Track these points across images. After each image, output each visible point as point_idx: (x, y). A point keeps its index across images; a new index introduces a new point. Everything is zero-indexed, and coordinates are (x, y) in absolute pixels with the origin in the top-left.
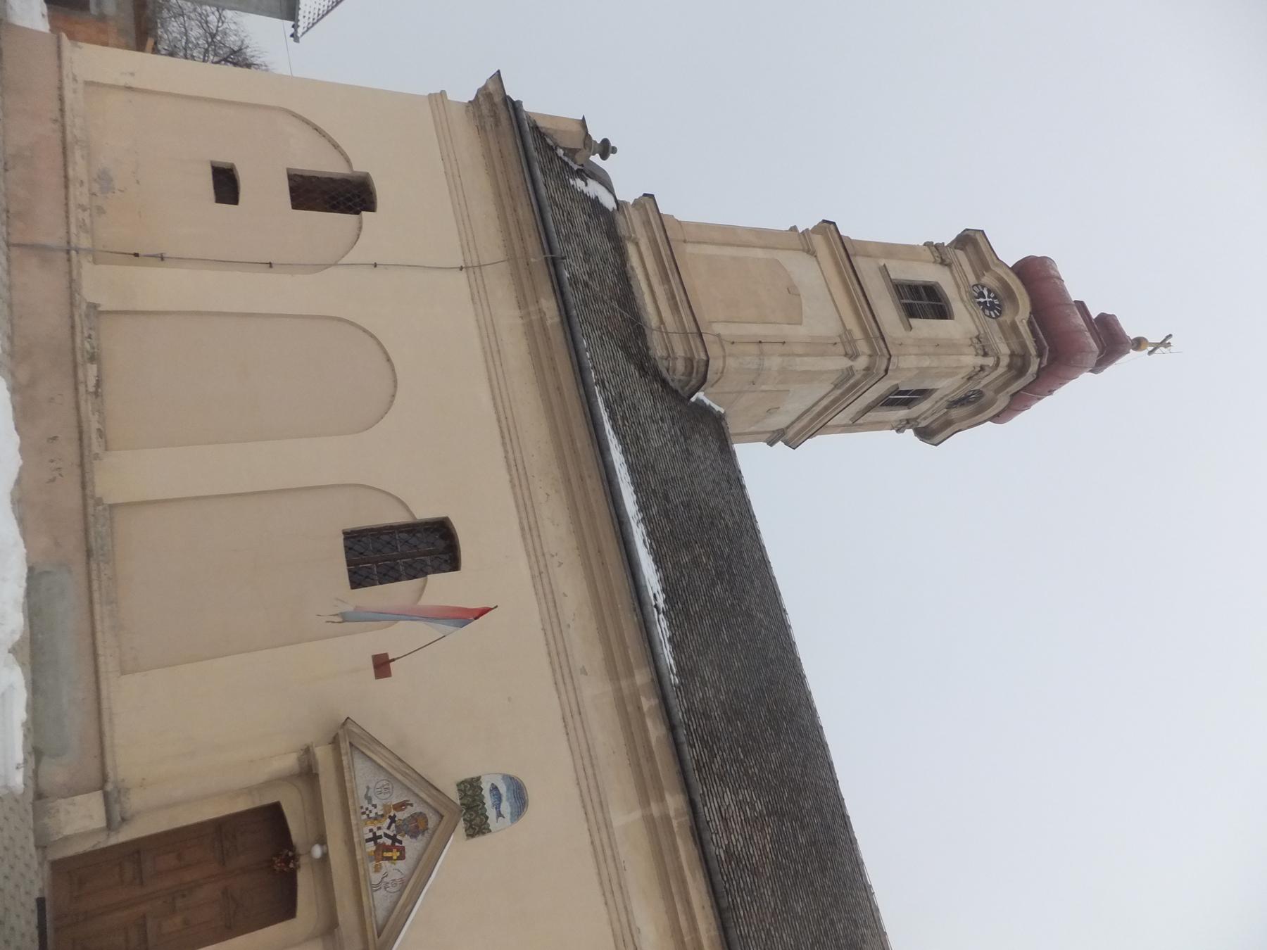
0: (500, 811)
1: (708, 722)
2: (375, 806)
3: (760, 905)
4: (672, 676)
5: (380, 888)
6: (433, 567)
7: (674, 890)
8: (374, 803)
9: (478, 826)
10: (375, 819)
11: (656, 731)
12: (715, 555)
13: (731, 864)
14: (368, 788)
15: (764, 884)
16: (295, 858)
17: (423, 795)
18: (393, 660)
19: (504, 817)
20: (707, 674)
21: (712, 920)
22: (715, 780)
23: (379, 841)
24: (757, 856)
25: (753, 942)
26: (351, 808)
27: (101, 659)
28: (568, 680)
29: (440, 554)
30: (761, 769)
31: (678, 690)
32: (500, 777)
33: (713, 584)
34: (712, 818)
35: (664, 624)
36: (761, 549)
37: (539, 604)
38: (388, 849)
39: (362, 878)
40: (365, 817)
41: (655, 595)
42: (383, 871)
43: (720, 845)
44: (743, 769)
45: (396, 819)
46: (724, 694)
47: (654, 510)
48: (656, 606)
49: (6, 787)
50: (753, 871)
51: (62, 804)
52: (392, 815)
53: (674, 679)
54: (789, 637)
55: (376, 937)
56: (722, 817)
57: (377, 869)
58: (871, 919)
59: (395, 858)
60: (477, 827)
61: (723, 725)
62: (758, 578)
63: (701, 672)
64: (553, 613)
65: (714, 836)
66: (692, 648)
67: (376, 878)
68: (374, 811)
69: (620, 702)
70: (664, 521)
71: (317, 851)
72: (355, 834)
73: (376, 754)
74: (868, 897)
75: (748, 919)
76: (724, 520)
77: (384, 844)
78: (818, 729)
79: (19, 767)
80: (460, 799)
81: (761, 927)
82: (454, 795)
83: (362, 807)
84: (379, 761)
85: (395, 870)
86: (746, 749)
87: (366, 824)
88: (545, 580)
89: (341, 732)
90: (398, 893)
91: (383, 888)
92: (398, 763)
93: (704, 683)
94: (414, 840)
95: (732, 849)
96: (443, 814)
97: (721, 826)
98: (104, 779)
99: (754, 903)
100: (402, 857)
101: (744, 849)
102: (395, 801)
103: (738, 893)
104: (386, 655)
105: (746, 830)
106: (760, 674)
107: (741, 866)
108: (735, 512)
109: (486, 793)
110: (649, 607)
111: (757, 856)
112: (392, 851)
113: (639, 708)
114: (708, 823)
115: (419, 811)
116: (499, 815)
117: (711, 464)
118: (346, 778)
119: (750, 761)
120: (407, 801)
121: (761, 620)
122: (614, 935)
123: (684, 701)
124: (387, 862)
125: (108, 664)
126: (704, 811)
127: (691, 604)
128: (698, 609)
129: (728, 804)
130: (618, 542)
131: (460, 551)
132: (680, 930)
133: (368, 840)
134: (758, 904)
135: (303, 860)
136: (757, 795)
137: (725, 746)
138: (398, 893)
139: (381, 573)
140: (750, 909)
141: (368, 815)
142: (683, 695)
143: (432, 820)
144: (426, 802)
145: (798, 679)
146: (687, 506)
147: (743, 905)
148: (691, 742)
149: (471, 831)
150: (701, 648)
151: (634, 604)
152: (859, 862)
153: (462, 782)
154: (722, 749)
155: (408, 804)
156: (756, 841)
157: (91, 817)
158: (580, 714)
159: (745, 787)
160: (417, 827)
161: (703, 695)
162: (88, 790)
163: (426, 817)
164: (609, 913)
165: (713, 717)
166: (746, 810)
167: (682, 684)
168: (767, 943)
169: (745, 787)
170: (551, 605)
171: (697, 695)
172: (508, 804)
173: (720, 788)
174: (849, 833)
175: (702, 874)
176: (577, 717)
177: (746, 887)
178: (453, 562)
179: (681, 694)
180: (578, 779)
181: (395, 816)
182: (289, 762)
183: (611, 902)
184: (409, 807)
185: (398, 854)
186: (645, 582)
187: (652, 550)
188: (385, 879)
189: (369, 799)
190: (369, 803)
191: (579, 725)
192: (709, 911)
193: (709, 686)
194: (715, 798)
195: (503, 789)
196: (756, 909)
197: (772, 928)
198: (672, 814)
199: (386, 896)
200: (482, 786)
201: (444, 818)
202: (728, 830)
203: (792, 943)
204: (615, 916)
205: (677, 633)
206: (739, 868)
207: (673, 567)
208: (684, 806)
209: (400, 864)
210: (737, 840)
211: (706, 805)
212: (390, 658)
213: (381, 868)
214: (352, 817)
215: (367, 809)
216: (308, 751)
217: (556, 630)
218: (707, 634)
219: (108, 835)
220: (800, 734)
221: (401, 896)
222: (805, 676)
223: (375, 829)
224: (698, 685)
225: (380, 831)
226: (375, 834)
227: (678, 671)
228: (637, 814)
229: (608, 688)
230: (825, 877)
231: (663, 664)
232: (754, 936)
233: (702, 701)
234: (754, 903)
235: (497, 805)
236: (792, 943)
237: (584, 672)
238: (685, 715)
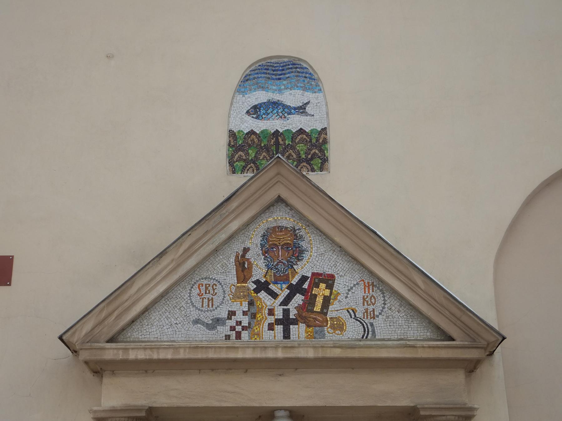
0: (295, 109)
2: (232, 314)
5: (372, 325)
8: (225, 315)
9: (310, 150)
14: (197, 322)
17: (234, 226)
19: (308, 103)
23: (292, 316)
26: (223, 355)
32: (239, 97)
40: (245, 335)
42: (344, 315)
45: (263, 280)
57: (339, 326)
59: (327, 292)
68: (239, 316)
72: (270, 354)
77: (298, 308)
82: (240, 179)
83: (228, 337)
87: (258, 334)
89: (84, 355)
90: (387, 295)
91: (372, 321)
92: (166, 260)
94: (306, 256)
100: (329, 280)
102: (232, 278)
109: (259, 126)
112: (315, 296)
116: (302, 110)
118: (169, 356)
120: (237, 257)
133: (287, 335)
141: (244, 328)
153: (231, 163)
155: (243, 256)
160: (286, 246)
163: (274, 228)
172: (287, 92)
181: (257, 282)
185: (323, 286)
188: (359, 315)
189: (218, 321)
190: (224, 324)
199: (388, 317)
209: (340, 285)
213: (338, 319)
214: (240, 355)
221: (394, 292)
223: (271, 319)
226: (278, 322)
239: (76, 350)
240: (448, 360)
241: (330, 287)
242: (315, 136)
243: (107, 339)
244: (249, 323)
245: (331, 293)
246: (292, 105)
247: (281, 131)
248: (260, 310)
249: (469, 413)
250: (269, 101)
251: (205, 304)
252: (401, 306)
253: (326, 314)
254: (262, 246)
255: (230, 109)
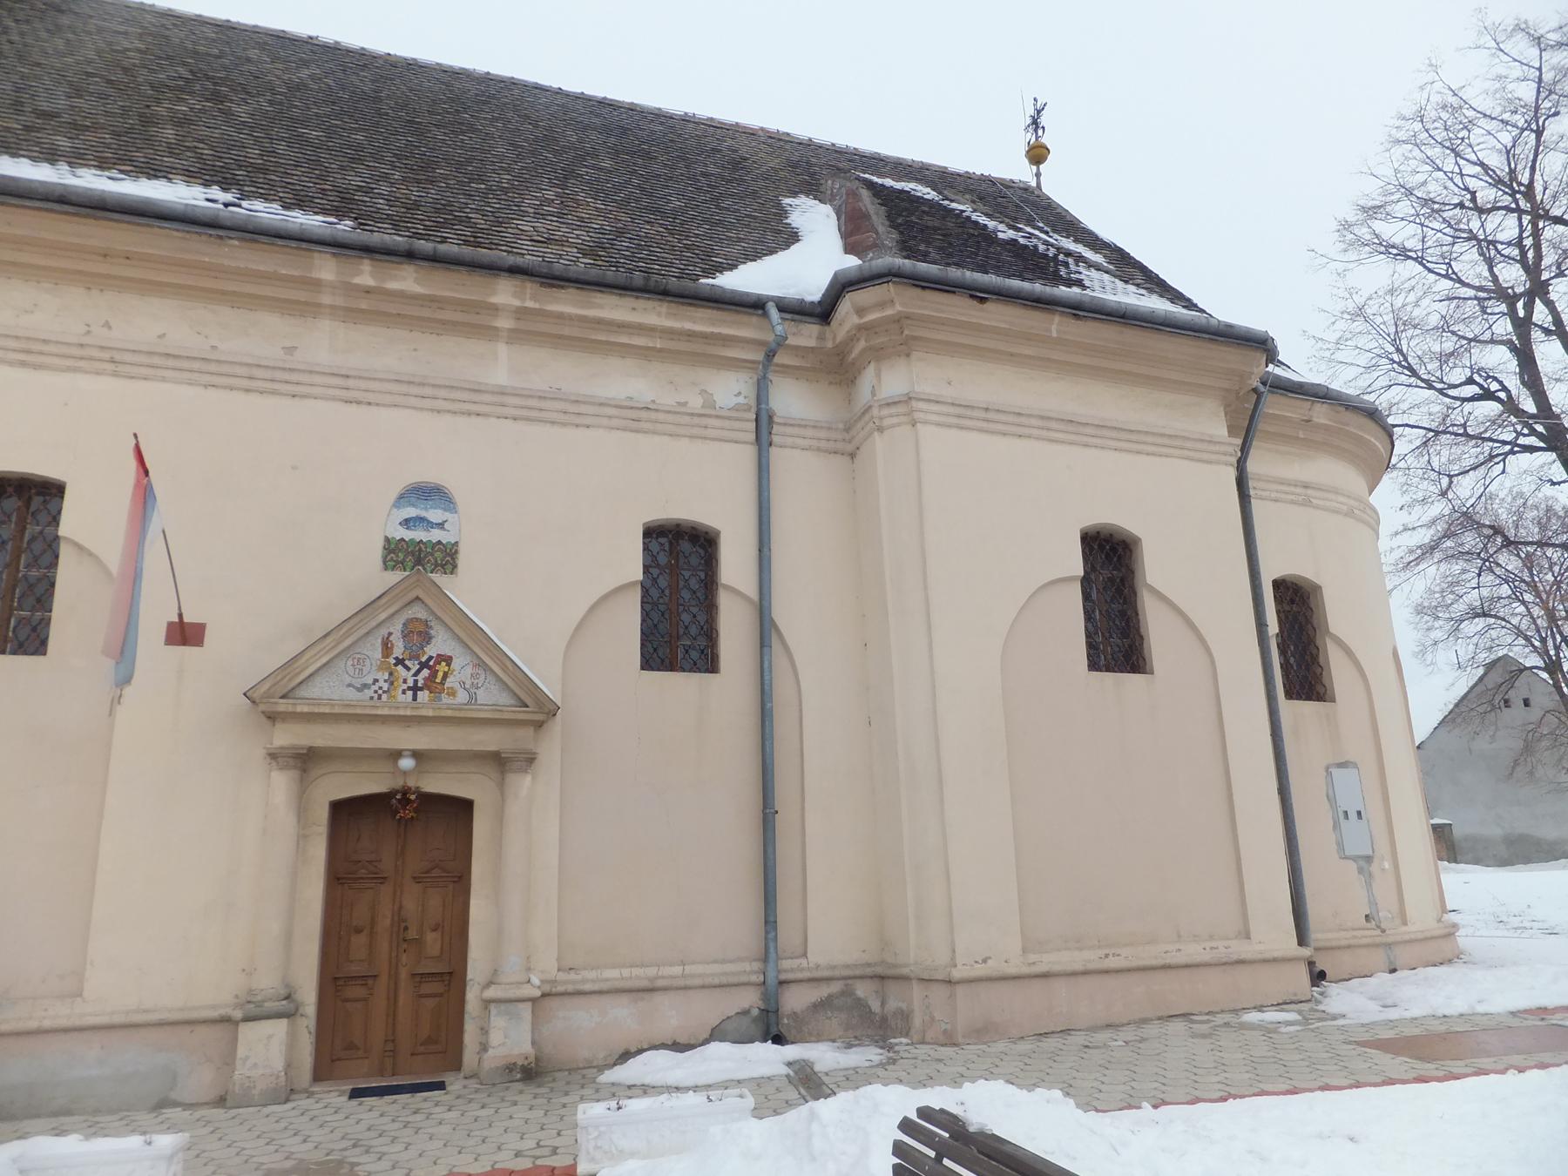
0: (436, 524)
1: (421, 208)
2: (376, 681)
3: (657, 243)
4: (338, 226)
5: (475, 693)
6: (49, 524)
7: (604, 338)
8: (371, 682)
10: (392, 683)
11: (407, 280)
12: (182, 90)
13: (600, 256)
14: (349, 685)
15: (638, 229)
16: (405, 792)
17: (383, 616)
18: (180, 616)
19: (446, 521)
20: (357, 181)
21: (650, 304)
22: (497, 231)
23: (419, 685)
24: (604, 223)
25: (691, 268)
26: (367, 711)
27: (47, 1024)
28: (294, 377)
29: (28, 508)
30: (508, 171)
31: (362, 227)
33: (228, 114)
34: (541, 254)
35: (258, 205)
36: (200, 21)
37: (164, 379)
38: (433, 674)
39: (457, 714)
40: (384, 697)
41: (208, 200)
42: (457, 686)
43: (574, 259)
44: (498, 193)
46: (393, 172)
47: (63, 142)
48: (226, 205)
49: (171, 1158)
50: (618, 234)
51: (241, 1072)
52: (394, 661)
53: (345, 225)
54: (351, 52)
55: (527, 709)
56: (545, 242)
58: (719, 131)
59: (446, 669)
60: (446, 558)
61: (433, 191)
62: (245, 49)
63: (350, 187)
64: (186, 364)
65: (561, 261)
66: (311, 185)
67: (462, 697)
69: (351, 315)
70: (89, 136)
71: (407, 763)
72: (401, 712)
73: (307, 667)
74: (694, 123)
75: (665, 264)
76: (128, 50)
77: (426, 679)
78: (487, 79)
79: (148, 1140)
80: (405, 570)
81: (679, 253)
82: (396, 576)
83: (372, 698)
84: (318, 664)
85: (461, 671)
86: (476, 177)
88: (128, 357)
89: (262, 707)
90: (488, 673)
92: (329, 640)
93: (368, 191)
94: (434, 641)
95: (585, 247)
96: (414, 596)
97: (554, 248)
98: (225, 1020)
99: (652, 249)
100: (448, 660)
101: (590, 234)
102: (378, 654)
103: (635, 261)
104: (170, 625)
105: (570, 222)
106: (387, 114)
107: (607, 245)
108: (122, 28)
109: (408, 535)
110: (221, 213)
111: (604, 223)
113: (368, 292)
114: (544, 261)
115: (401, 626)
116: (441, 525)
117: (17, 21)
118: (327, 711)
119: (492, 179)
120: (383, 641)
121: (312, 76)
122: (624, 429)
123: (380, 225)
124: (448, 680)
125: (62, 1014)
126: (529, 260)
127: (246, 157)
128: (257, 152)
129: (532, 229)
130: (96, 218)
131: (32, 474)
132: (648, 348)
133: (415, 699)
134: (655, 245)
135: (411, 783)
136: (536, 190)
137: (462, 200)
138: (488, 673)
139: (34, 607)
140: (657, 256)
141: (384, 692)
142: (372, 223)
143: (418, 612)
144: (393, 615)
145: (413, 69)
146: (78, 92)
147: (648, 261)
148: (439, 240)
149: (449, 567)
150: (317, 172)
151: (211, 235)
152: (656, 112)
153: (385, 562)
154: (463, 206)
155: (388, 638)
156: (587, 216)
157: (270, 1037)
158: (348, 377)
159: (521, 200)
161: (384, 199)
162: (234, 1041)
164: (599, 427)
165: (417, 199)
166: (548, 211)
167: (356, 219)
168: (697, 254)
169: (521, 200)
170: (171, 363)
171: (379, 206)
172: (432, 511)
173: (510, 230)
174: (621, 107)
175: (599, 295)
176: (351, 383)
177: (632, 250)
178: (46, 493)
179: (371, 225)
180: (432, 410)
181: (396, 658)
182: (282, 783)
183: (588, 421)
184: (391, 639)
185: (443, 664)
186: (181, 204)
187: (131, 174)
189: (365, 686)
191: (363, 384)
192: (641, 303)
193: (374, 186)
194: (519, 241)
195: (411, 512)
196: (659, 250)
197: (685, 242)
198: (517, 303)
200: (398, 538)
201: (420, 596)
202: (561, 242)
203: (708, 227)
204: (605, 421)
205: (281, 195)
206: (609, 248)
207: (172, 154)
208: (515, 283)
209: (456, 664)
210: (578, 237)
211: (524, 254)
212: (177, 620)
214: (379, 712)
215: (376, 692)
216: (273, 756)
217: (213, 367)
218: (300, 155)
219: (302, 1015)
220: (485, 103)
221: (492, 671)
222: (415, 60)
223: (405, 686)
224: (368, 199)
225: (408, 681)
226: (409, 689)
227: (337, 216)
228: (502, 349)
229: (326, 325)
230: (656, 158)
231: (320, 231)
232: (685, 265)
233: (391, 203)
234: (652, 249)
235: (431, 525)
236: (708, 227)
237: (290, 350)
238: (400, 233)
239: (286, 995)
240: (522, 720)
241: (449, 665)
242: (449, 546)
243: (281, 695)
244: (388, 689)
245: (449, 669)
246: (434, 522)
247: (424, 540)
248: (397, 679)
249: (533, 756)
250: (417, 517)
251: (356, 673)
252: (496, 681)
253: (444, 684)
254: (403, 631)
255: (387, 520)
